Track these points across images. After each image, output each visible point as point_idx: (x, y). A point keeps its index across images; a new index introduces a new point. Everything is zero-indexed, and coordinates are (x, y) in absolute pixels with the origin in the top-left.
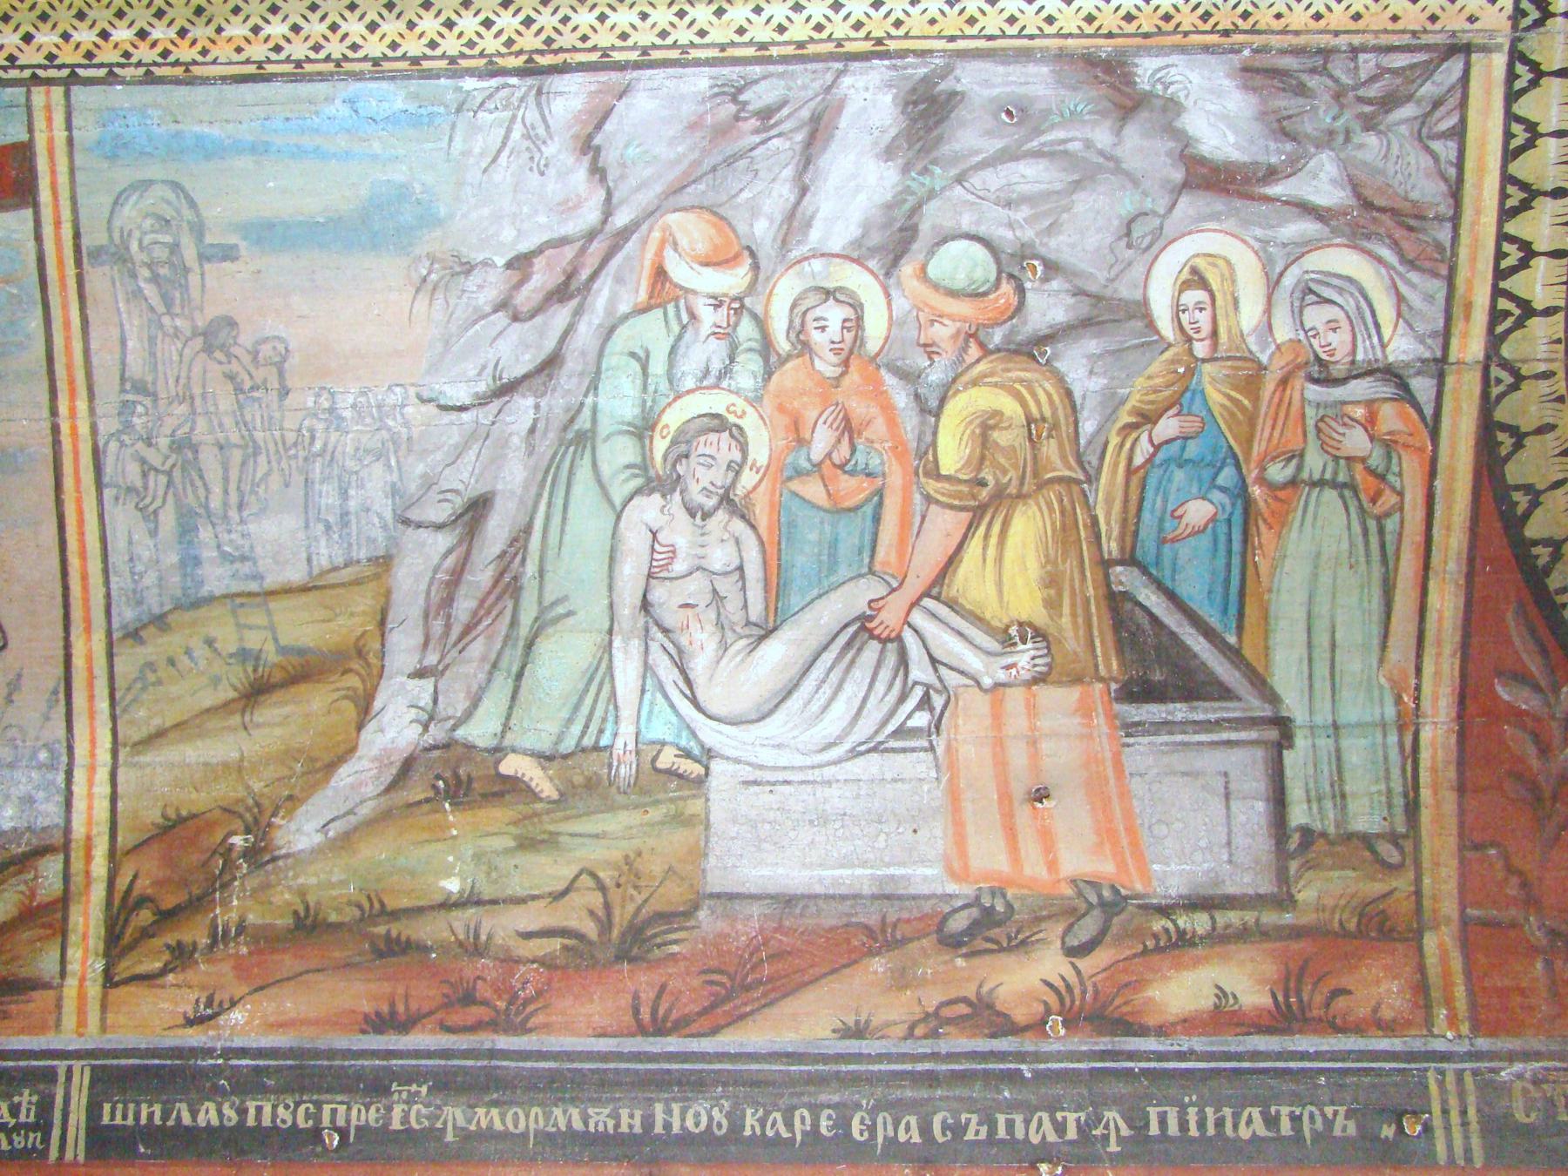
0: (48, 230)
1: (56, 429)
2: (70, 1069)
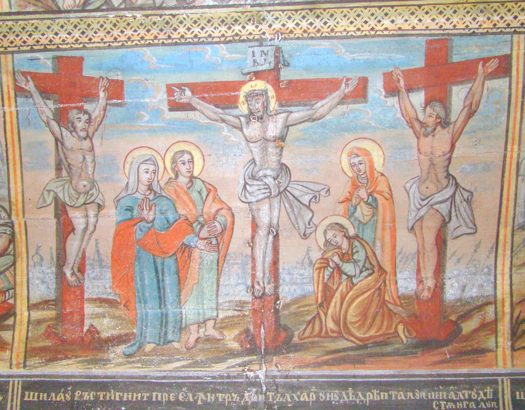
0: (514, 86)
1: (505, 156)
2: (502, 380)
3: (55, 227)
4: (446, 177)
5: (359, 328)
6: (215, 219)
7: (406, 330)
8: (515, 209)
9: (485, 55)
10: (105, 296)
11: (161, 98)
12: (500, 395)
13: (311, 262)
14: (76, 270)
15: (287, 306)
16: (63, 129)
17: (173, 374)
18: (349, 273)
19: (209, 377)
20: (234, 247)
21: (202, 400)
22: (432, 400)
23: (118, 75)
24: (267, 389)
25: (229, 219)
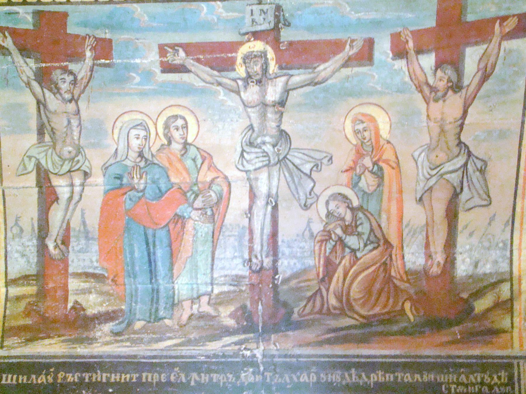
2: (518, 363)
3: (36, 196)
4: (458, 145)
5: (363, 305)
6: (210, 187)
7: (413, 308)
9: (502, 13)
10: (91, 271)
11: (151, 59)
12: (516, 378)
13: (312, 235)
14: (59, 242)
15: (286, 281)
16: (46, 91)
17: (165, 353)
18: (353, 247)
19: (202, 356)
20: (230, 218)
21: (195, 380)
22: (441, 384)
23: (106, 33)
24: (264, 369)
25: (225, 189)
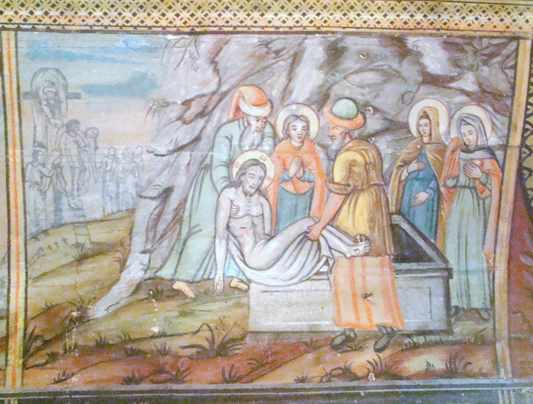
1: (7, 160)
8: (25, 218)
